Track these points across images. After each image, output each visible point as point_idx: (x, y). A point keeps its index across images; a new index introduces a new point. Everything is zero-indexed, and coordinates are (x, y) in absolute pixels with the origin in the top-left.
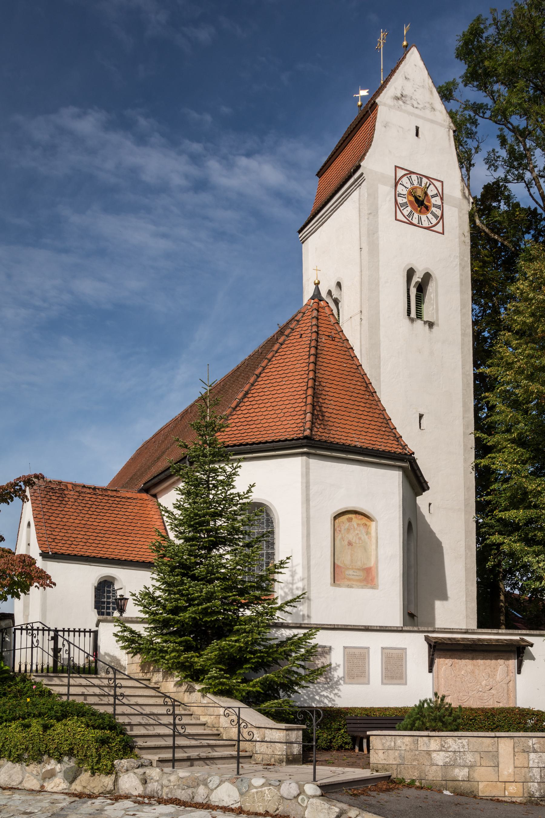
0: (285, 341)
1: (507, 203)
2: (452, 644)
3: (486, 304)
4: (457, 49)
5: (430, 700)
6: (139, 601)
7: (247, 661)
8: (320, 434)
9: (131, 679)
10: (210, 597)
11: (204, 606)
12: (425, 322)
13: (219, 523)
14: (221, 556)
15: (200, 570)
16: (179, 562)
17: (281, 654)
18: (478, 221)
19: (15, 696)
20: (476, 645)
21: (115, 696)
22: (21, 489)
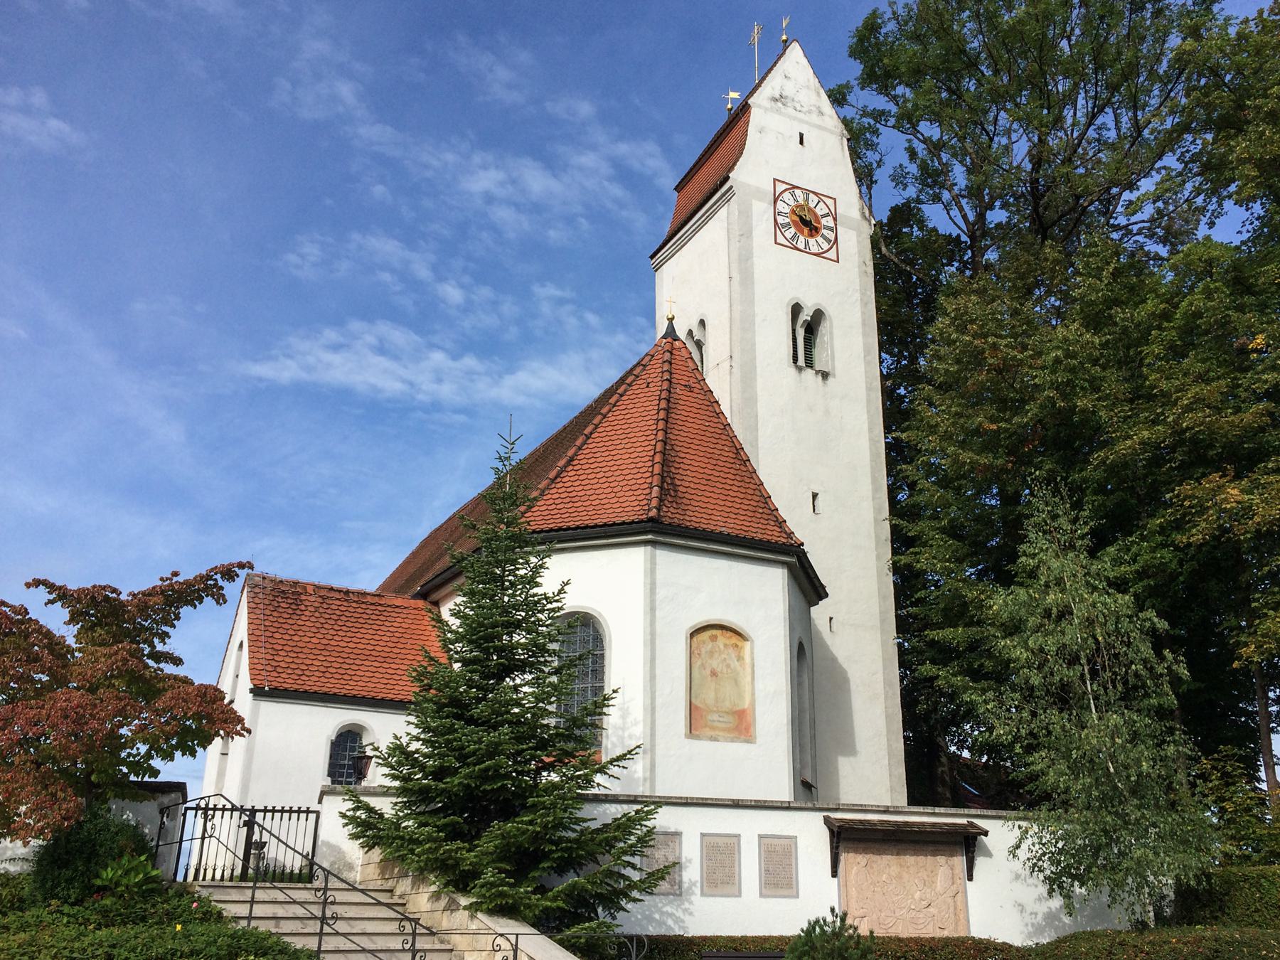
0: (626, 391)
1: (920, 229)
2: (865, 830)
3: (900, 352)
4: (850, 47)
5: (825, 921)
6: (385, 759)
7: (546, 856)
8: (671, 515)
9: (355, 889)
10: (494, 750)
11: (483, 766)
12: (817, 372)
13: (516, 638)
14: (516, 689)
15: (479, 710)
16: (451, 697)
17: (600, 844)
18: (884, 249)
19: (160, 923)
20: (902, 832)
21: (323, 920)
22: (216, 585)
